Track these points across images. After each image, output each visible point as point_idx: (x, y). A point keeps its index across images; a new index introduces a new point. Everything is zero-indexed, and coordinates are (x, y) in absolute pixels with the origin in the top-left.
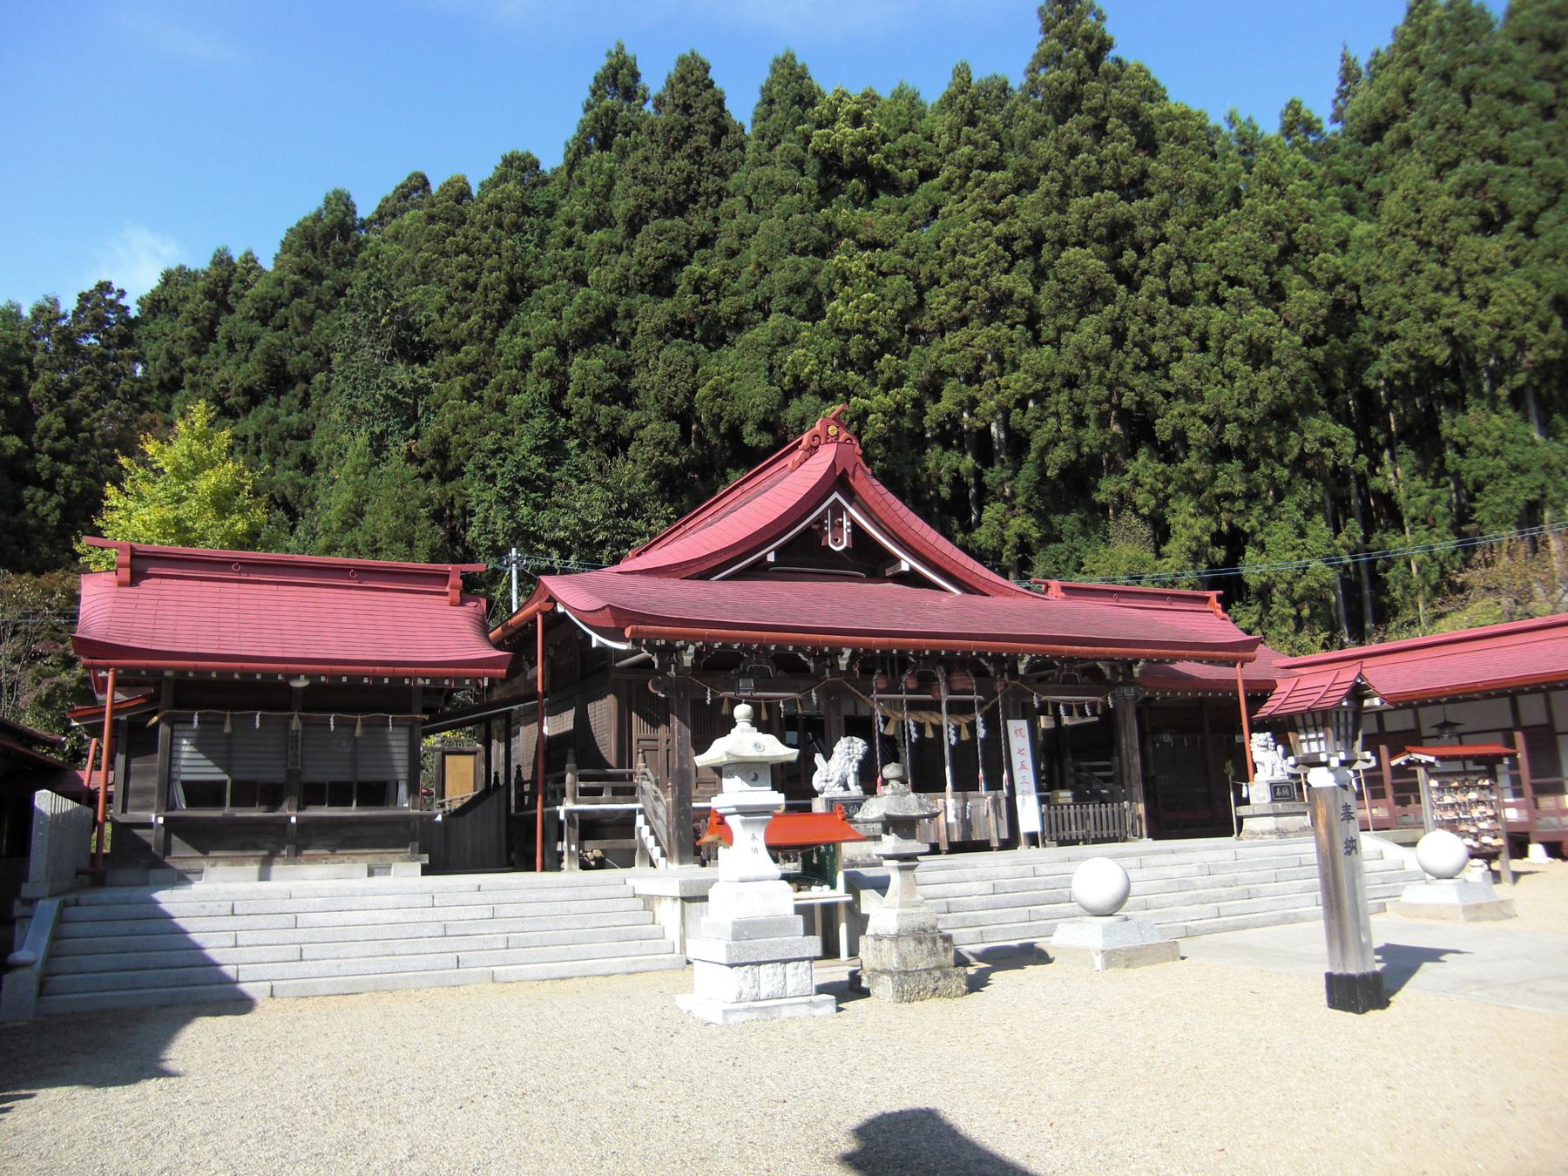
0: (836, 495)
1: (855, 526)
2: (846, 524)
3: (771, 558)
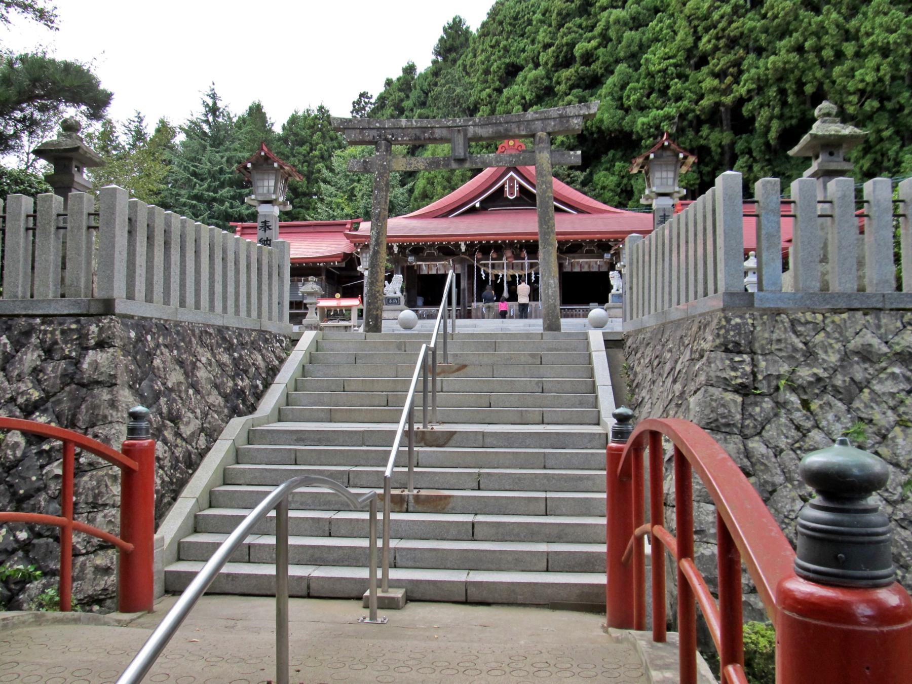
0: (512, 173)
1: (521, 186)
2: (516, 186)
3: (478, 205)
